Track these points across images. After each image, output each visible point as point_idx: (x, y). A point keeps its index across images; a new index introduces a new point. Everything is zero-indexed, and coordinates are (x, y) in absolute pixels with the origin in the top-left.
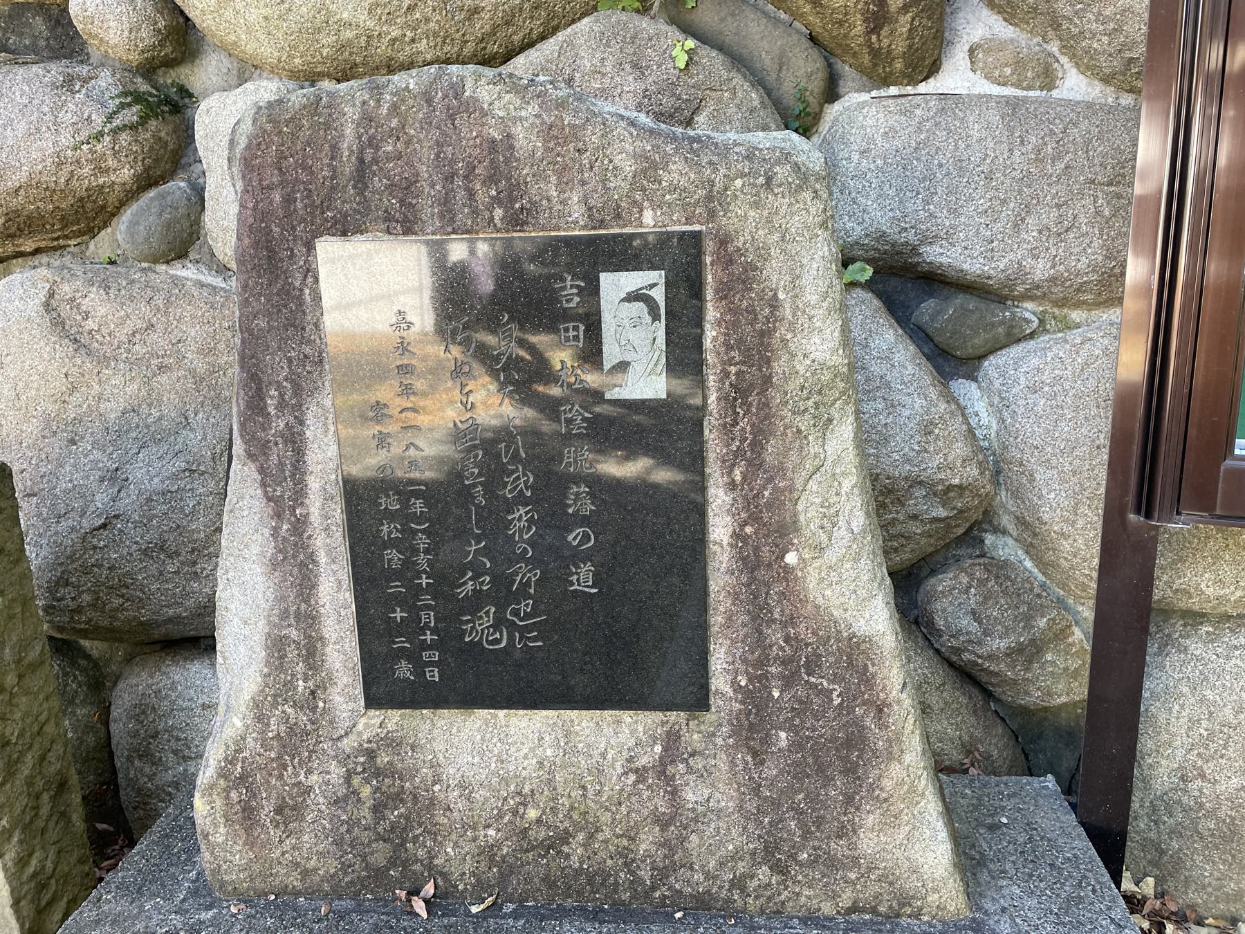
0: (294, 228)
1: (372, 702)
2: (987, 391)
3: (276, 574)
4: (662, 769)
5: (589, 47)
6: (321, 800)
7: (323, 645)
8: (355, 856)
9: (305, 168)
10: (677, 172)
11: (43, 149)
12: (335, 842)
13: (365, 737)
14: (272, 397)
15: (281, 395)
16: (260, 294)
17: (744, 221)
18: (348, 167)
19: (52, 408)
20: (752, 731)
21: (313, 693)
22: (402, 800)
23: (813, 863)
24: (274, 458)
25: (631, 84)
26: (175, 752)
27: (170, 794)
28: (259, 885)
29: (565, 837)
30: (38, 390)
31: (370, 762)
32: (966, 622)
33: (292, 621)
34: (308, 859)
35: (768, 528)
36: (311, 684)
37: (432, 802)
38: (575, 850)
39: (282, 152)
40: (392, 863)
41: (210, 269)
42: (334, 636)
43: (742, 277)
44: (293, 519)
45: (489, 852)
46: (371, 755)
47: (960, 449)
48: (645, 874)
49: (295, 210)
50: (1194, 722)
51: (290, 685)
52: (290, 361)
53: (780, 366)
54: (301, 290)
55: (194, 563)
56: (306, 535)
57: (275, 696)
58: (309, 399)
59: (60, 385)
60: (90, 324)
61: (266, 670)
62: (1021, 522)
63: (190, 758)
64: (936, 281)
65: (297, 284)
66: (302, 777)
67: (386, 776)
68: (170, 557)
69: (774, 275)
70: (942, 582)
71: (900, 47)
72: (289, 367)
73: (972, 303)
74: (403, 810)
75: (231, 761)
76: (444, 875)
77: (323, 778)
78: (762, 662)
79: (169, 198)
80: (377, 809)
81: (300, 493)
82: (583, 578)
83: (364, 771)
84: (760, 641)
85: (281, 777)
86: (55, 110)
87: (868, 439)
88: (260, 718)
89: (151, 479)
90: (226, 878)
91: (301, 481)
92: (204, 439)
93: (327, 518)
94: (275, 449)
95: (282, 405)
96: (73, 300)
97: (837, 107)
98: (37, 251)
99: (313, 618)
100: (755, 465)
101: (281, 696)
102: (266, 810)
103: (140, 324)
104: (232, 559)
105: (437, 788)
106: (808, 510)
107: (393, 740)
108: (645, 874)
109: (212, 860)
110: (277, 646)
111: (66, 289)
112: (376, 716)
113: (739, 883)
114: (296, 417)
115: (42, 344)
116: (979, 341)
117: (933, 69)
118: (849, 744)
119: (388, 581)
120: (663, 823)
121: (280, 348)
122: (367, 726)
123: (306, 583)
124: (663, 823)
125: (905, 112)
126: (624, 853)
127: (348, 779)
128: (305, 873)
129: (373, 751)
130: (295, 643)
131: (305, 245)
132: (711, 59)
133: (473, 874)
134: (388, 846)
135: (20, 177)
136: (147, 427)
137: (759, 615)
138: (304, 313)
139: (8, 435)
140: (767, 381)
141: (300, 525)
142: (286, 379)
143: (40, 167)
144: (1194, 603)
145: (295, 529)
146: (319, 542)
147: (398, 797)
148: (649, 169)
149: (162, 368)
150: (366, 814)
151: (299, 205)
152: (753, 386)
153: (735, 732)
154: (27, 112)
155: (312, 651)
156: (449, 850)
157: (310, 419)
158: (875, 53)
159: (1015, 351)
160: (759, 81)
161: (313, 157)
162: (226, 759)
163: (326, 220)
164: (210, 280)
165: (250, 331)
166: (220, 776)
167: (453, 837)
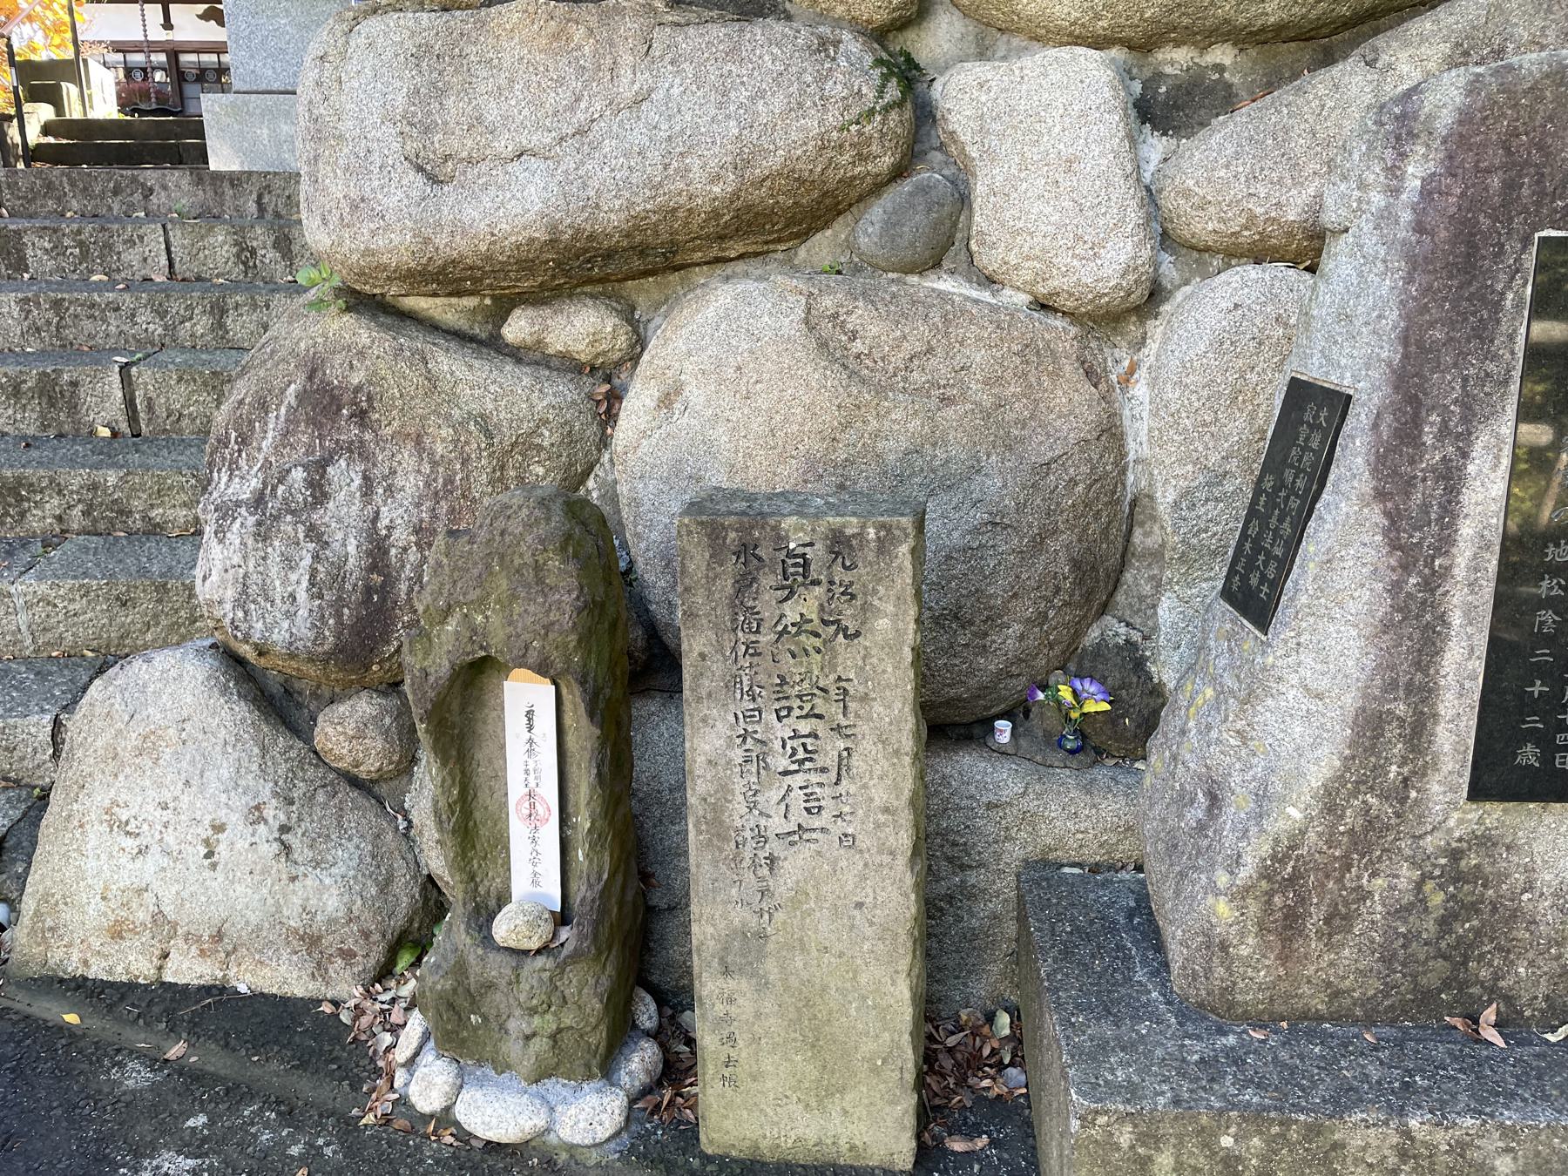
0: (1511, 219)
1: (1479, 792)
3: (1386, 637)
5: (1524, 13)
6: (1379, 908)
7: (1435, 723)
8: (1404, 976)
9: (1541, 147)
11: (808, 130)
12: (1382, 959)
13: (1457, 834)
14: (1432, 424)
15: (1445, 422)
16: (1445, 299)
19: (819, 447)
21: (1405, 780)
22: (1477, 911)
24: (1417, 497)
26: (950, 860)
27: (941, 909)
28: (1279, 1008)
30: (801, 425)
33: (1401, 693)
34: (1344, 978)
36: (1406, 770)
37: (1515, 914)
39: (1516, 128)
40: (1446, 985)
41: (970, 282)
42: (1451, 713)
44: (1427, 571)
46: (1455, 855)
49: (1518, 197)
51: (1380, 770)
52: (1465, 380)
54: (1503, 294)
55: (986, 634)
56: (1441, 590)
57: (1357, 782)
58: (1481, 427)
59: (831, 418)
60: (858, 347)
61: (1347, 752)
63: (970, 867)
65: (1499, 287)
66: (1364, 881)
67: (1468, 882)
68: (963, 627)
72: (1464, 387)
74: (1475, 923)
75: (1279, 859)
76: (1508, 999)
79: (933, 193)
80: (1445, 923)
81: (1446, 542)
83: (1441, 876)
85: (1340, 880)
86: (821, 79)
89: (949, 534)
90: (1239, 998)
91: (1452, 524)
92: (1005, 486)
93: (1476, 570)
94: (1420, 486)
95: (1444, 432)
96: (835, 316)
98: (741, 257)
99: (1430, 691)
101: (1365, 783)
103: (919, 347)
104: (1312, 620)
105: (1526, 896)
107: (1490, 839)
109: (1226, 976)
110: (1370, 727)
111: (828, 302)
112: (1474, 812)
114: (1459, 448)
115: (809, 369)
119: (1534, 649)
121: (1455, 365)
122: (1460, 822)
127: (1419, 885)
128: (1337, 994)
129: (1462, 852)
130: (1389, 726)
131: (1521, 241)
133: (1547, 998)
134: (1447, 964)
135: (774, 162)
136: (934, 471)
138: (1498, 321)
139: (756, 478)
141: (1434, 581)
142: (1455, 402)
143: (799, 152)
145: (1427, 583)
147: (1473, 908)
149: (946, 401)
150: (1430, 927)
151: (1525, 191)
154: (784, 81)
155: (1418, 731)
156: (1521, 970)
157: (1478, 449)
161: (1554, 135)
162: (1273, 857)
163: (1556, 211)
164: (975, 294)
165: (1420, 344)
166: (1262, 876)
167: (1530, 955)
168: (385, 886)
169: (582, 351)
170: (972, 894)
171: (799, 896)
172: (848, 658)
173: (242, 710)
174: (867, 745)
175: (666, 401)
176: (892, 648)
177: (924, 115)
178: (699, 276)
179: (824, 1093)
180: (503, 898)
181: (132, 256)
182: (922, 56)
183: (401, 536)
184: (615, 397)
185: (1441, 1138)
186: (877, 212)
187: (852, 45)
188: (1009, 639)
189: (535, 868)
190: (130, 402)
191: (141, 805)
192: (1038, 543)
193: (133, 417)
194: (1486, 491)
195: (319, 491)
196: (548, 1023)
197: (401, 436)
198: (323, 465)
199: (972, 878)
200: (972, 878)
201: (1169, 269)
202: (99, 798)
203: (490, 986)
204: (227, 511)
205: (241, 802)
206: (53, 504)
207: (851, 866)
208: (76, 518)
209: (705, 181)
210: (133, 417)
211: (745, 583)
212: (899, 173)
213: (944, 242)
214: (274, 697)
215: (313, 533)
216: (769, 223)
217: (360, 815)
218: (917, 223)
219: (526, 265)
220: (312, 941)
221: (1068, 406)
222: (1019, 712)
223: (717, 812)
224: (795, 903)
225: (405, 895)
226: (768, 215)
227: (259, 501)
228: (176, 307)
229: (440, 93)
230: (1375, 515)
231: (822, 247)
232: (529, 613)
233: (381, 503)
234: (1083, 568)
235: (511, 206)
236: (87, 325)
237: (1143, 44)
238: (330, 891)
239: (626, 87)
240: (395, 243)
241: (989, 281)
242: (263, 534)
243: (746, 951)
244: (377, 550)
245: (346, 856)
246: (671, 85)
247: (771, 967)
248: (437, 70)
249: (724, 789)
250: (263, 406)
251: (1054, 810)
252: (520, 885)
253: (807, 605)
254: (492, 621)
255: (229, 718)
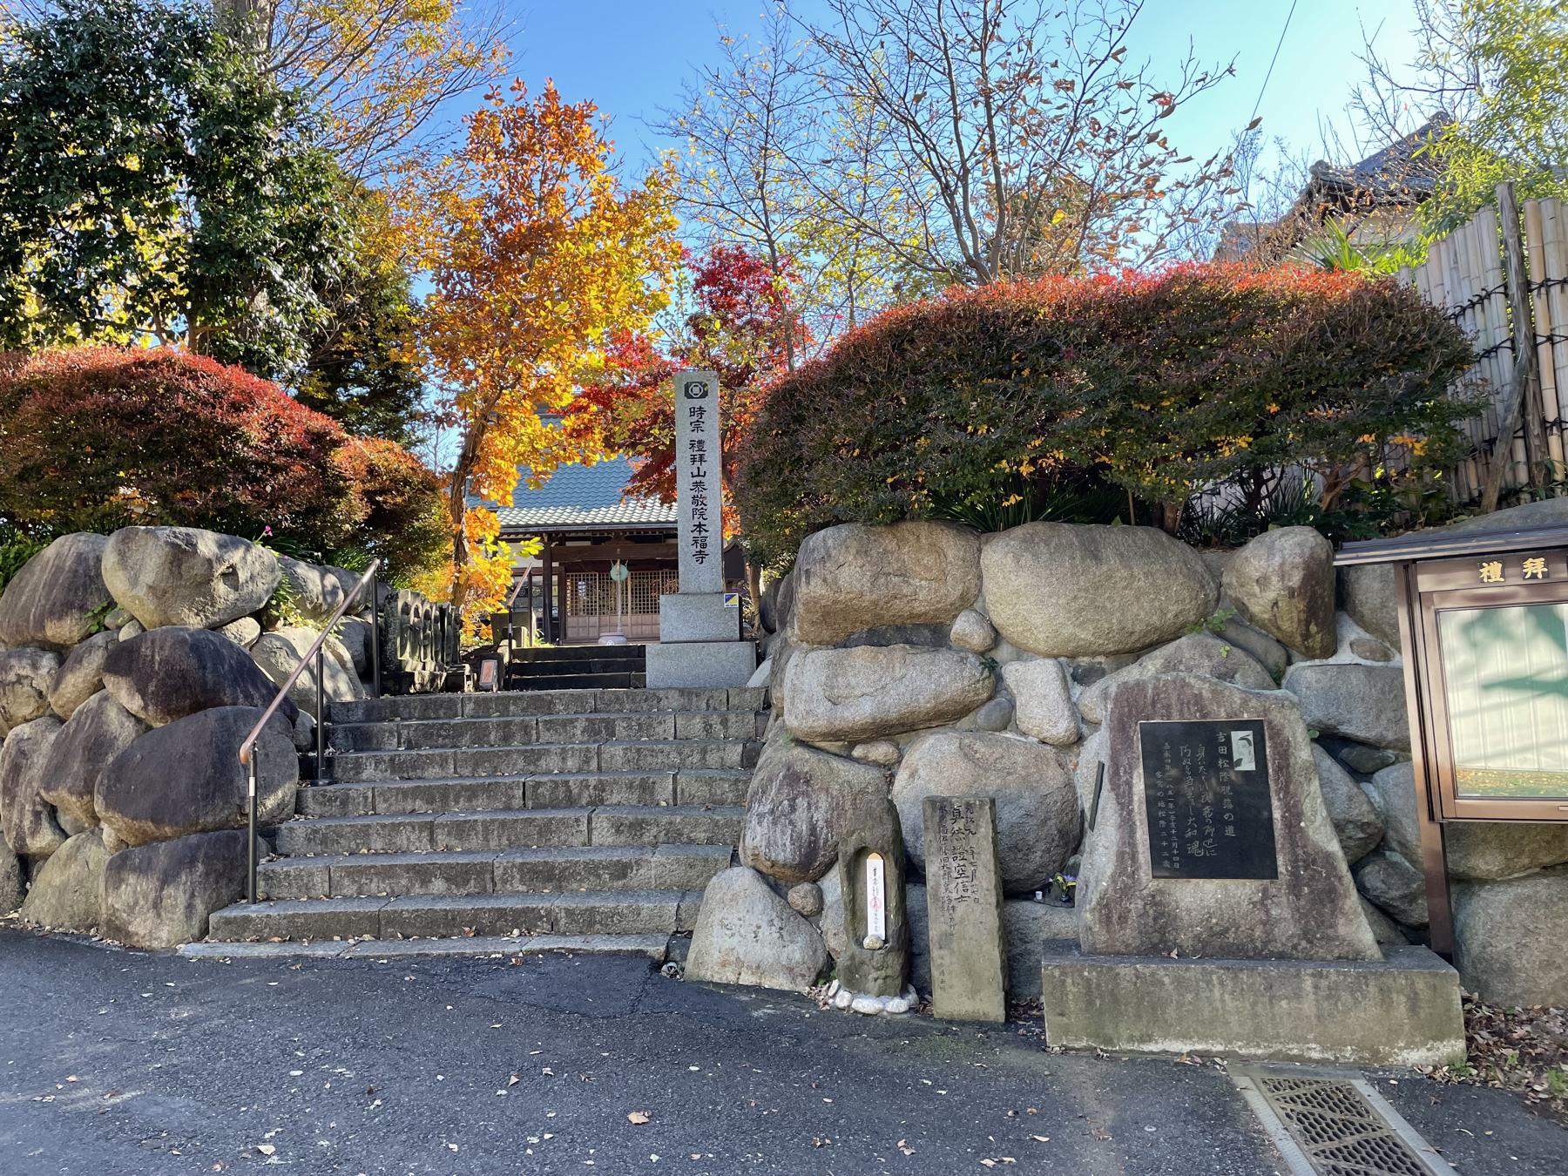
2: (1377, 787)
4: (1262, 902)
10: (1253, 703)
17: (1276, 717)
18: (1149, 700)
19: (966, 790)
20: (1295, 887)
23: (1322, 938)
25: (1206, 663)
29: (1227, 930)
31: (1154, 900)
32: (1379, 884)
35: (1294, 815)
38: (1231, 936)
40: (1161, 941)
43: (1277, 733)
45: (1197, 937)
47: (1365, 807)
48: (1259, 944)
50: (1485, 924)
53: (1292, 761)
59: (970, 779)
62: (1400, 843)
64: (1348, 741)
69: (1287, 732)
70: (1368, 869)
71: (1318, 645)
73: (1364, 750)
77: (1136, 906)
78: (1297, 861)
80: (1155, 919)
81: (1131, 802)
82: (1230, 831)
84: (1294, 854)
87: (1329, 804)
88: (1114, 882)
97: (1292, 668)
100: (1287, 793)
102: (1115, 917)
106: (1307, 806)
108: (1259, 944)
110: (1121, 856)
112: (1155, 882)
113: (1295, 947)
116: (1370, 766)
117: (1335, 652)
118: (1330, 892)
120: (1264, 923)
123: (1132, 833)
124: (1264, 923)
125: (1324, 673)
126: (1250, 936)
128: (1127, 946)
130: (1126, 855)
132: (1238, 652)
137: (1293, 843)
140: (1288, 766)
141: (1130, 812)
144: (1478, 873)
146: (1137, 817)
147: (1162, 914)
148: (1245, 702)
150: (1150, 920)
152: (1284, 767)
153: (1289, 887)
158: (1307, 648)
159: (1387, 770)
160: (1259, 661)
168: (815, 952)
169: (881, 759)
170: (1029, 953)
171: (962, 920)
172: (973, 840)
173: (765, 887)
174: (980, 868)
175: (912, 775)
176: (985, 838)
177: (1000, 679)
178: (922, 733)
179: (974, 993)
180: (866, 935)
181: (659, 729)
182: (998, 659)
183: (821, 823)
184: (893, 776)
185: (1147, 971)
186: (983, 710)
187: (972, 658)
188: (1037, 857)
189: (876, 926)
190: (675, 791)
191: (732, 919)
192: (1044, 822)
193: (675, 798)
194: (1139, 786)
195: (793, 809)
196: (883, 973)
197: (821, 789)
198: (794, 799)
199: (1029, 946)
200: (1029, 946)
201: (1085, 729)
202: (717, 916)
203: (863, 963)
204: (761, 816)
205: (766, 918)
206: (654, 831)
207: (978, 909)
208: (662, 837)
209: (925, 703)
210: (675, 798)
211: (942, 818)
212: (990, 698)
213: (1007, 721)
214: (775, 882)
215: (791, 822)
216: (946, 716)
217: (805, 926)
218: (996, 716)
219: (864, 730)
220: (791, 970)
221: (1053, 777)
222: (1046, 888)
223: (936, 891)
224: (962, 922)
225: (821, 959)
226: (946, 713)
227: (772, 812)
228: (687, 751)
229: (836, 676)
230: (1112, 795)
231: (965, 722)
232: (878, 832)
233: (815, 812)
234: (1063, 833)
235: (860, 712)
236: (649, 759)
237: (1073, 656)
238: (796, 952)
239: (898, 674)
240: (821, 724)
241: (1024, 734)
242: (775, 823)
243: (947, 939)
244: (813, 829)
245: (801, 940)
246: (912, 673)
247: (954, 945)
248: (835, 669)
249: (938, 884)
250: (771, 780)
251: (1057, 920)
252: (871, 931)
253: (960, 824)
254: (867, 835)
255: (761, 889)
